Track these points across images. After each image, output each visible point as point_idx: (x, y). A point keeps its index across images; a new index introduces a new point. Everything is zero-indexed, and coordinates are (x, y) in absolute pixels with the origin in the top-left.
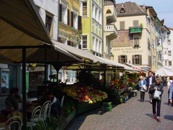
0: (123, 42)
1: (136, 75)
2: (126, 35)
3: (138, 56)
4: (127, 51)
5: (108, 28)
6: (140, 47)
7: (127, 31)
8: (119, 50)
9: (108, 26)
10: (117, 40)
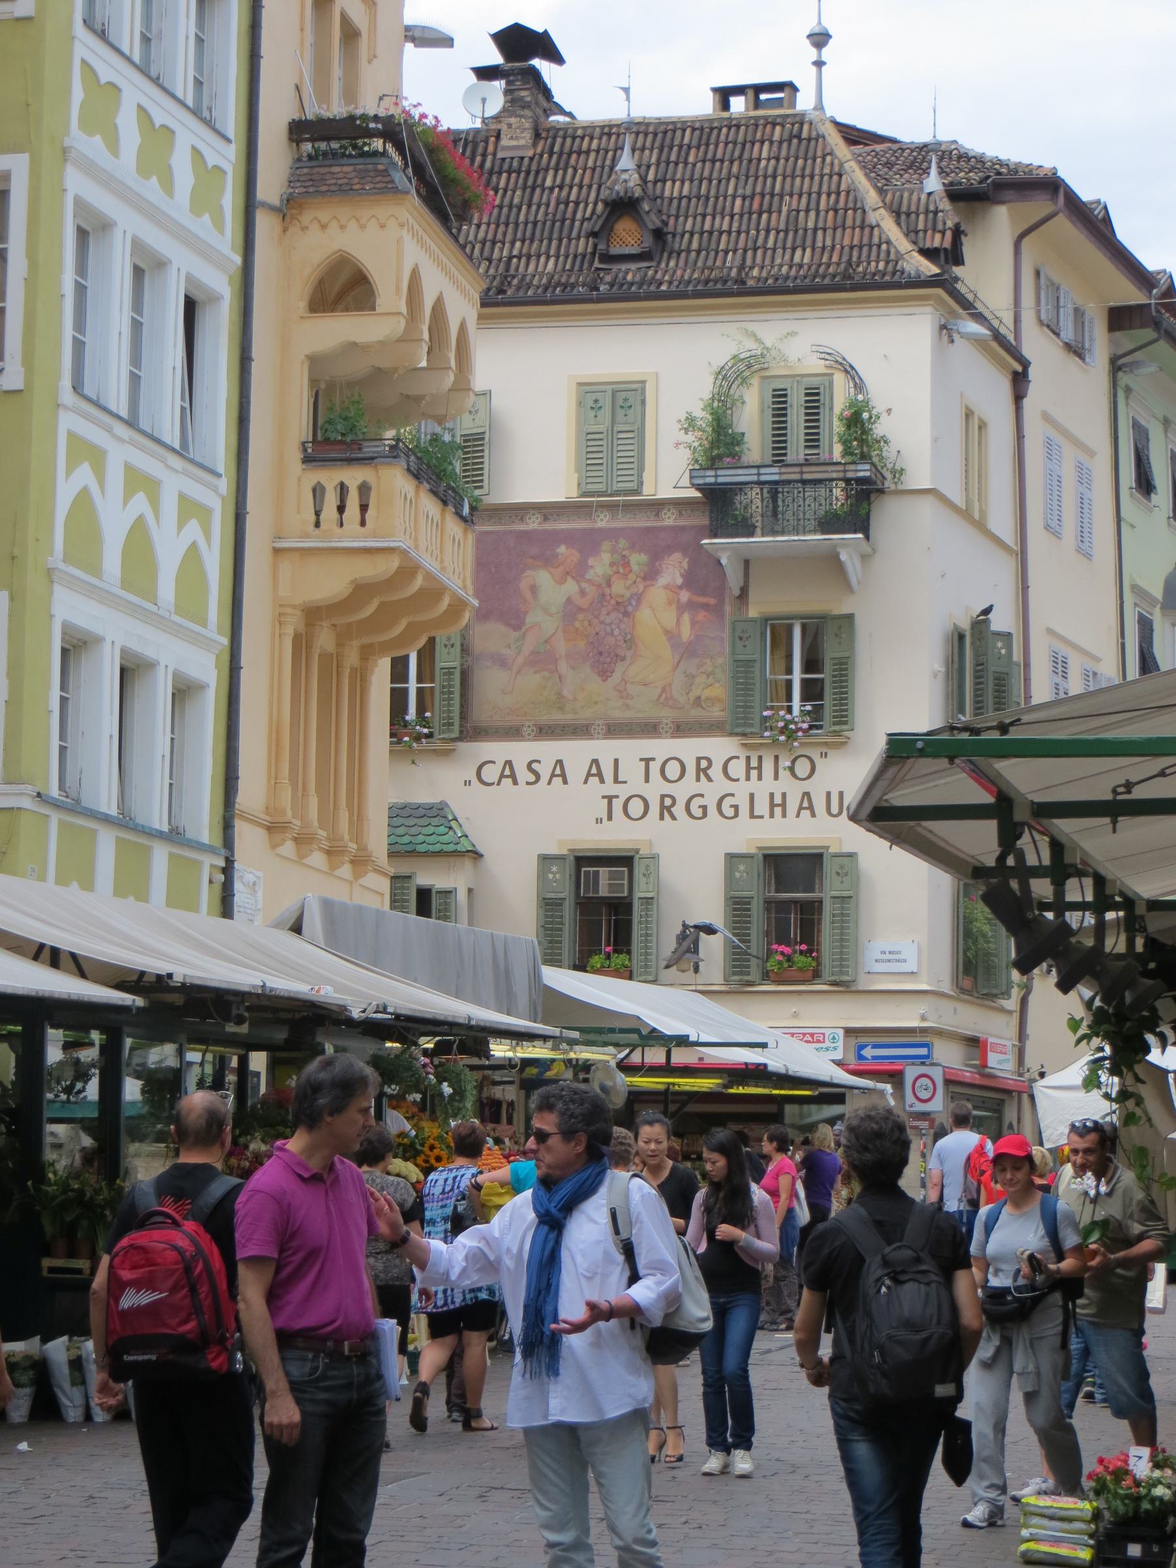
2: (651, 575)
3: (624, 861)
4: (655, 790)
7: (669, 519)
8: (560, 771)
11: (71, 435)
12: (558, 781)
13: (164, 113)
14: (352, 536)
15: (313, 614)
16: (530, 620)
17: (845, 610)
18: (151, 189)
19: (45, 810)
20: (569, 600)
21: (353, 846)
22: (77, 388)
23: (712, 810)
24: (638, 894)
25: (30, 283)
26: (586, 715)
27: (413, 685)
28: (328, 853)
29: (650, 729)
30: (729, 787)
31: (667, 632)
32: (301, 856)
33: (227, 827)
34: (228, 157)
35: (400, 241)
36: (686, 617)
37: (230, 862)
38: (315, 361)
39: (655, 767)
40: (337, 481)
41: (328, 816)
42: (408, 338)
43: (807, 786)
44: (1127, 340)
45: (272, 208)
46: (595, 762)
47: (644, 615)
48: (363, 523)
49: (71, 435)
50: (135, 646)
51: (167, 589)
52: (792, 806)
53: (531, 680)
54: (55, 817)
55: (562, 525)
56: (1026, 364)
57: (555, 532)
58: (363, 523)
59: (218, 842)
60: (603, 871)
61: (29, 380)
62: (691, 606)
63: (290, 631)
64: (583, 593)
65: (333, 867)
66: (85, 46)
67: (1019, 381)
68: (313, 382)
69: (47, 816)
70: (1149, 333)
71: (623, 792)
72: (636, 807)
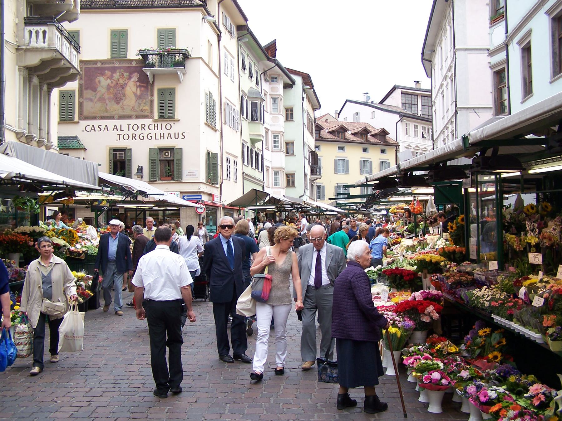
0: (118, 103)
2: (129, 78)
3: (171, 149)
4: (131, 132)
6: (178, 120)
8: (107, 128)
9: (34, 29)
10: (98, 96)
26: (113, 114)
29: (129, 117)
30: (150, 132)
39: (131, 127)
53: (99, 105)
64: (112, 83)
71: (123, 133)
72: (126, 137)
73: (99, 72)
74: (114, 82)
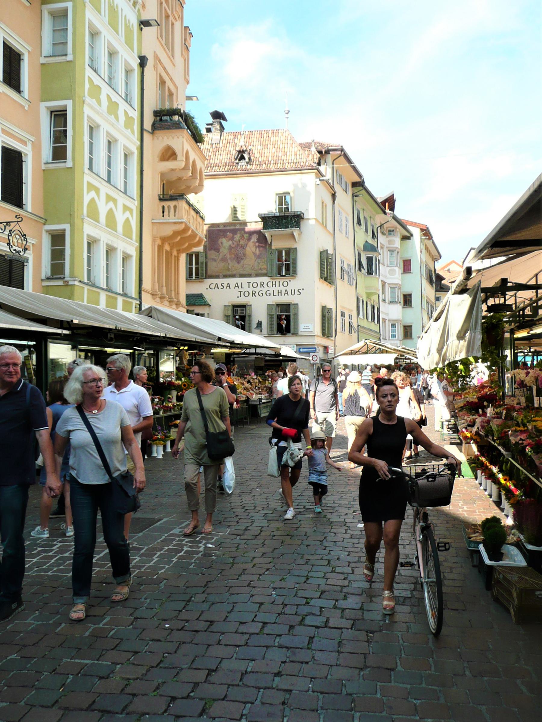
0: (239, 263)
1: (528, 449)
2: (249, 239)
3: (244, 306)
4: (251, 290)
5: (163, 212)
8: (229, 286)
10: (221, 257)
11: (88, 182)
12: (228, 288)
13: (115, 98)
14: (172, 219)
15: (164, 240)
16: (221, 250)
17: (295, 247)
18: (112, 118)
19: (82, 285)
20: (230, 246)
21: (176, 300)
22: (91, 168)
23: (264, 294)
24: (247, 314)
25: (74, 137)
26: (234, 272)
27: (194, 266)
28: (170, 302)
29: (250, 275)
30: (268, 289)
31: (253, 253)
32: (162, 302)
33: (140, 293)
34: (135, 115)
35: (183, 142)
36: (258, 249)
37: (141, 302)
38: (162, 175)
39: (251, 284)
40: (168, 205)
41: (169, 291)
42: (186, 168)
43: (286, 288)
44: (356, 189)
45: (149, 132)
46: (237, 283)
47: (248, 249)
48: (175, 216)
49: (88, 182)
50: (110, 243)
51: (120, 228)
52: (283, 293)
53: (222, 264)
54: (86, 288)
55: (228, 228)
56: (335, 193)
57: (227, 229)
58: (175, 216)
59: (137, 297)
60: (239, 309)
61: (74, 164)
62: (259, 246)
63: (157, 243)
64: (233, 244)
65: (171, 305)
66: (89, 72)
67: (334, 196)
68: (162, 180)
69: (83, 287)
70: (361, 188)
71: (243, 290)
72: (247, 294)
73: (222, 234)
74: (236, 243)
